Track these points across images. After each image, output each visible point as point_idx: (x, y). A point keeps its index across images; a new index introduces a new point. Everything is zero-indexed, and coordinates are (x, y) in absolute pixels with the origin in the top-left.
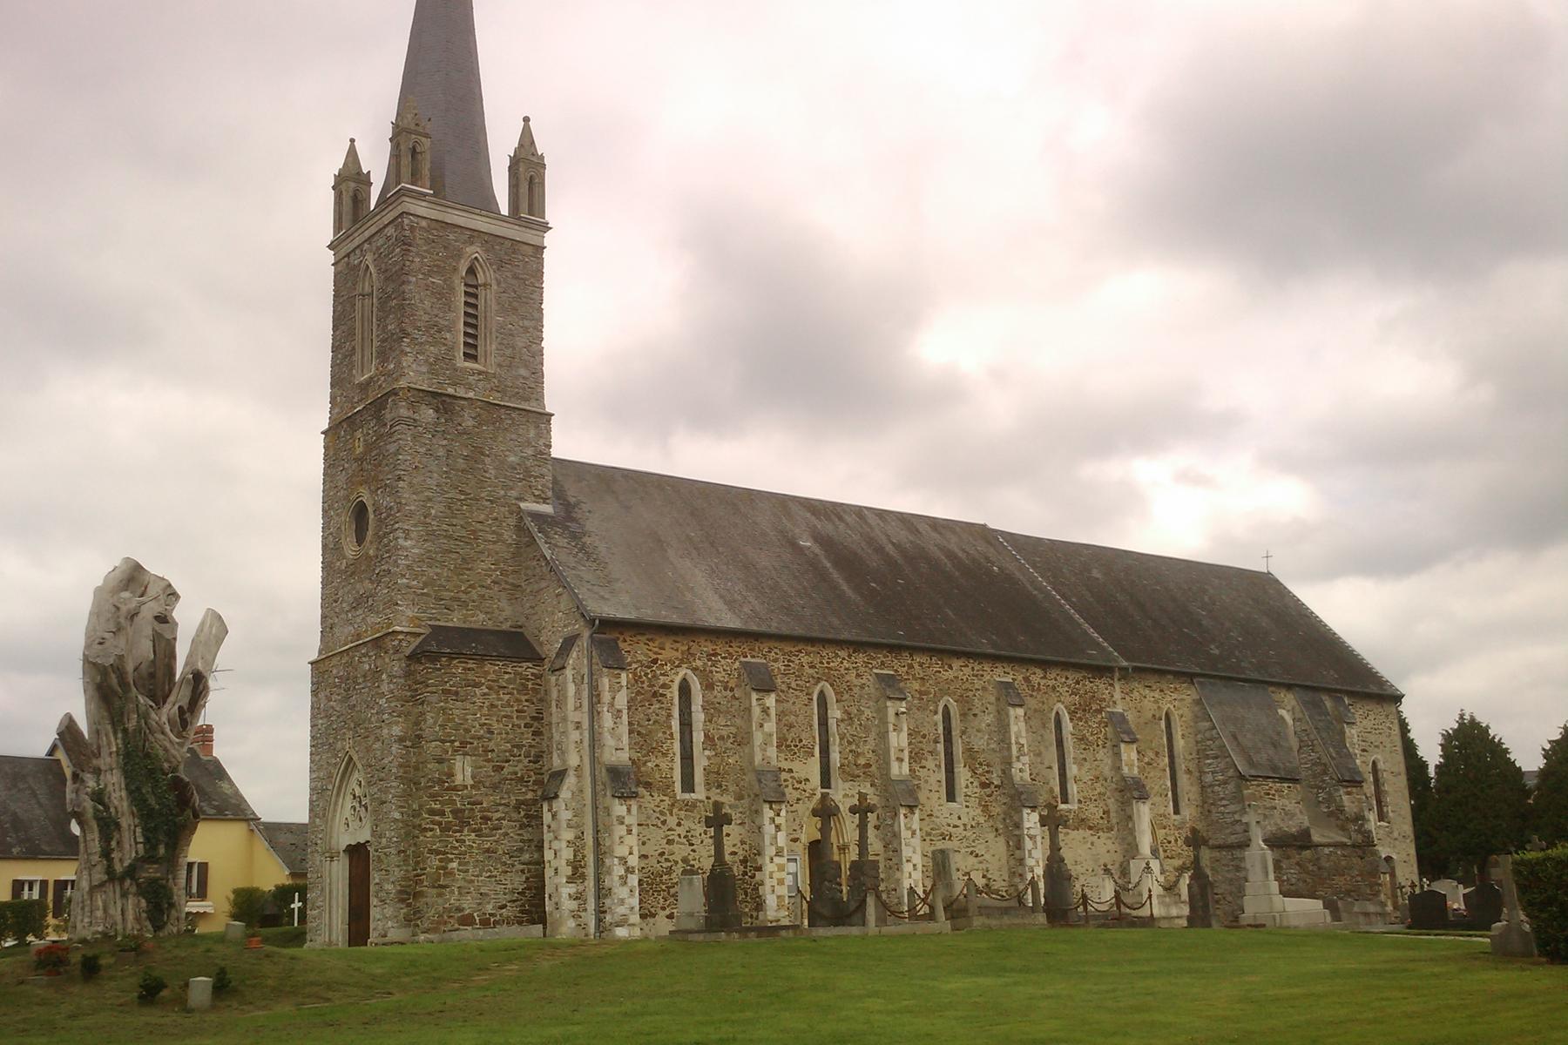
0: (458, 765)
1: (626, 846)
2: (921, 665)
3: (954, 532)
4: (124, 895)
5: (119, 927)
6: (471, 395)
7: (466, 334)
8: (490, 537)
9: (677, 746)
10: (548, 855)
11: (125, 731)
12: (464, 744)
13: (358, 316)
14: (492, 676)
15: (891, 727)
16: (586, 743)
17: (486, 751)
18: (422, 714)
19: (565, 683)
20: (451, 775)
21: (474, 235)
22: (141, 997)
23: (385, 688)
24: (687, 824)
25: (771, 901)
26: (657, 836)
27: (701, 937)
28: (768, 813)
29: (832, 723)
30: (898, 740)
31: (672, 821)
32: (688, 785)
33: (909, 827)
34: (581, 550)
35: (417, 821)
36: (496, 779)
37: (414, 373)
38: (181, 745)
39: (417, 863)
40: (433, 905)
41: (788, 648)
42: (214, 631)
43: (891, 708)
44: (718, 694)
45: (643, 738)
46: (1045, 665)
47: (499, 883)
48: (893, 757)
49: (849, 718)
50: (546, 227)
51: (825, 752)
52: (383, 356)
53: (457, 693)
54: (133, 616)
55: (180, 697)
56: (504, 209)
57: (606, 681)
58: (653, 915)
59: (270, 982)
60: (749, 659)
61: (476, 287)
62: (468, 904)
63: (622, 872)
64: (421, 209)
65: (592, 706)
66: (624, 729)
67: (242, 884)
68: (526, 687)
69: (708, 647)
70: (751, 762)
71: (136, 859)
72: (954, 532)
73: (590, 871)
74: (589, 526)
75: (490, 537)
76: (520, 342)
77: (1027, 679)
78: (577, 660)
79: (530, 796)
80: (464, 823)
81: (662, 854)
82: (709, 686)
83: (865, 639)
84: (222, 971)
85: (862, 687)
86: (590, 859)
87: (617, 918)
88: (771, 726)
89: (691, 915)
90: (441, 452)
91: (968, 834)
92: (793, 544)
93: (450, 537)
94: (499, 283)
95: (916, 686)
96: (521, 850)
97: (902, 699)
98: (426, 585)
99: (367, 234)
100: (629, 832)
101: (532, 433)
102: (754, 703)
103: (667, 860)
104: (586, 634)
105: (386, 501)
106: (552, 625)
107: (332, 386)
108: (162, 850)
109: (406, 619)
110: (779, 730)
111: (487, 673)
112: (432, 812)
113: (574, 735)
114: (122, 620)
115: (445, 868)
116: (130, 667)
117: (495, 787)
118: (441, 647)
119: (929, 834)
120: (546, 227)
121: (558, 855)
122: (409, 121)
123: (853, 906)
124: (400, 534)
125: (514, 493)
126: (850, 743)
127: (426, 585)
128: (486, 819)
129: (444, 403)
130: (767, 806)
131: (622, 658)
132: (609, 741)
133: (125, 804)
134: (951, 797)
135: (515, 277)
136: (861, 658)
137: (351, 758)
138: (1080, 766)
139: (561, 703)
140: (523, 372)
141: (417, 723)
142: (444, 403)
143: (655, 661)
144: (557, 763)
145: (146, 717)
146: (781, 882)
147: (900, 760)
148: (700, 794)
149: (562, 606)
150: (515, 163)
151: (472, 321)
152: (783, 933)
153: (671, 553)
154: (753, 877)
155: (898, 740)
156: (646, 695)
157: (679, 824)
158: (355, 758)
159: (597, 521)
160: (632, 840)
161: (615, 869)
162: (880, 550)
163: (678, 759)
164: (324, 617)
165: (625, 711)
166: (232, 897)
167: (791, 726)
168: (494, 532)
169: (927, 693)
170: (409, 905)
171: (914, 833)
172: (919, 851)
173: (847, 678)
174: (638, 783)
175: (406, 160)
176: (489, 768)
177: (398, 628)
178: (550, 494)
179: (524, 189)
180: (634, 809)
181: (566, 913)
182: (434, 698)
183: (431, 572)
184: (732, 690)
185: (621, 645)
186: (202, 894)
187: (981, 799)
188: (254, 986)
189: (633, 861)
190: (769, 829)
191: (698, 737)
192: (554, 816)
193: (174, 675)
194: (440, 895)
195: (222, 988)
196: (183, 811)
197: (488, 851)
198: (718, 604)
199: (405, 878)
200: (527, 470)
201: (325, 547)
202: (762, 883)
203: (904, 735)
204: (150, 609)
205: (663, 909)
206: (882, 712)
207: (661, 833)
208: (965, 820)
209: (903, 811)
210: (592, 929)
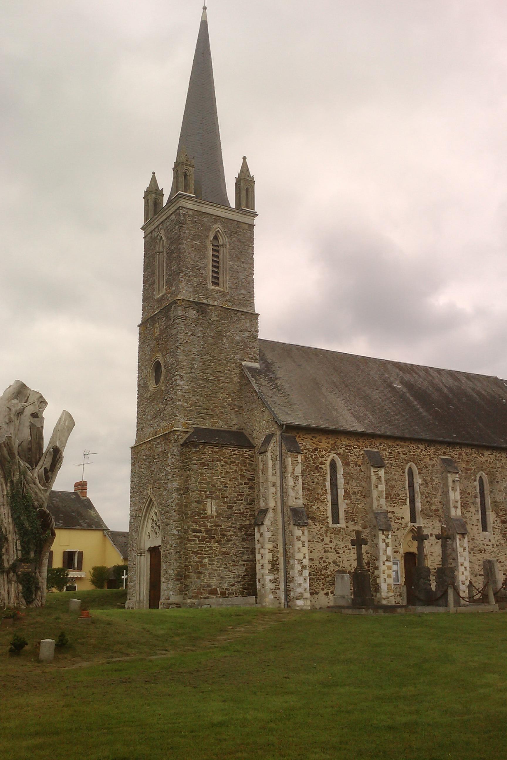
0: (209, 504)
1: (302, 553)
2: (466, 453)
3: (479, 381)
4: (9, 582)
5: (6, 602)
6: (216, 303)
7: (213, 271)
8: (226, 380)
9: (329, 497)
10: (258, 557)
11: (12, 482)
12: (212, 493)
13: (157, 264)
14: (227, 456)
16: (279, 494)
17: (224, 497)
18: (189, 476)
19: (267, 460)
20: (205, 510)
21: (217, 219)
22: (11, 651)
23: (169, 461)
24: (335, 542)
25: (384, 587)
26: (319, 547)
27: (350, 611)
28: (381, 536)
29: (416, 486)
30: (455, 496)
31: (327, 540)
32: (336, 519)
33: (461, 545)
34: (275, 387)
35: (186, 535)
36: (230, 512)
37: (185, 292)
38: (46, 491)
39: (186, 559)
40: (195, 582)
41: (391, 443)
42: (67, 423)
43: (451, 478)
44: (352, 468)
45: (310, 492)
47: (231, 571)
48: (452, 506)
49: (426, 483)
50: (255, 215)
52: (169, 284)
53: (208, 465)
54: (20, 413)
55: (45, 462)
56: (233, 205)
57: (289, 459)
58: (317, 593)
59: (93, 641)
60: (369, 449)
61: (218, 246)
62: (214, 583)
63: (300, 568)
64: (189, 205)
65: (282, 473)
66: (300, 486)
67: (98, 564)
68: (245, 463)
69: (346, 442)
70: (371, 507)
71: (17, 560)
72: (479, 381)
73: (281, 567)
74: (279, 375)
75: (226, 380)
76: (242, 276)
78: (273, 447)
79: (247, 523)
80: (211, 537)
82: (346, 464)
83: (434, 438)
84: (62, 635)
85: (433, 465)
86: (281, 560)
87: (297, 595)
88: (382, 487)
89: (343, 597)
90: (200, 334)
91: (495, 550)
92: (390, 386)
93: (204, 380)
94: (230, 244)
95: (464, 465)
96: (243, 553)
97: (458, 473)
98: (192, 405)
99: (161, 220)
100: (304, 545)
102: (372, 474)
103: (324, 562)
104: (278, 433)
105: (171, 360)
106: (260, 428)
107: (143, 301)
108: (32, 555)
109: (181, 424)
110: (386, 489)
111: (224, 454)
112: (194, 531)
113: (272, 490)
114: (12, 416)
115: (201, 562)
116: (16, 444)
117: (228, 517)
118: (200, 439)
119: (472, 550)
120: (255, 215)
121: (264, 557)
122: (183, 159)
123: (439, 594)
124: (178, 378)
125: (239, 357)
127: (192, 405)
128: (224, 535)
129: (202, 308)
130: (380, 533)
131: (299, 447)
132: (291, 493)
133: (11, 526)
134: (485, 529)
135: (239, 241)
136: (432, 450)
137: (151, 500)
139: (265, 471)
140: (243, 291)
141: (186, 481)
142: (202, 308)
143: (316, 449)
144: (262, 505)
145: (25, 474)
146: (389, 577)
148: (342, 524)
149: (265, 419)
150: (239, 181)
151: (216, 264)
152: (399, 610)
153: (324, 390)
154: (373, 572)
155: (455, 496)
156: (312, 468)
157: (331, 542)
158: (153, 499)
159: (283, 372)
160: (305, 550)
161: (297, 568)
162: (439, 390)
163: (330, 504)
164: (138, 423)
165: (300, 477)
166: (92, 571)
167: (393, 487)
168: (228, 377)
169: (470, 469)
170: (181, 583)
171: (464, 549)
172: (467, 559)
173: (425, 460)
174: (308, 517)
175: (181, 179)
176: (225, 506)
177: (177, 429)
178: (258, 357)
179: (243, 194)
180: (306, 532)
181: (268, 591)
182: (195, 467)
183: (194, 399)
184: (360, 466)
185: (297, 439)
186: (80, 568)
187: (501, 530)
188: (82, 644)
189: (306, 562)
190: (382, 545)
191: (341, 492)
192: (261, 535)
193: (41, 449)
194: (198, 577)
195: (62, 645)
196: (45, 531)
197: (224, 553)
198: (350, 418)
199: (180, 567)
200: (245, 344)
201: (139, 386)
202: (378, 576)
203: (458, 493)
204: (29, 410)
205: (323, 590)
206: (445, 480)
208: (493, 541)
209: (458, 536)
210: (283, 600)
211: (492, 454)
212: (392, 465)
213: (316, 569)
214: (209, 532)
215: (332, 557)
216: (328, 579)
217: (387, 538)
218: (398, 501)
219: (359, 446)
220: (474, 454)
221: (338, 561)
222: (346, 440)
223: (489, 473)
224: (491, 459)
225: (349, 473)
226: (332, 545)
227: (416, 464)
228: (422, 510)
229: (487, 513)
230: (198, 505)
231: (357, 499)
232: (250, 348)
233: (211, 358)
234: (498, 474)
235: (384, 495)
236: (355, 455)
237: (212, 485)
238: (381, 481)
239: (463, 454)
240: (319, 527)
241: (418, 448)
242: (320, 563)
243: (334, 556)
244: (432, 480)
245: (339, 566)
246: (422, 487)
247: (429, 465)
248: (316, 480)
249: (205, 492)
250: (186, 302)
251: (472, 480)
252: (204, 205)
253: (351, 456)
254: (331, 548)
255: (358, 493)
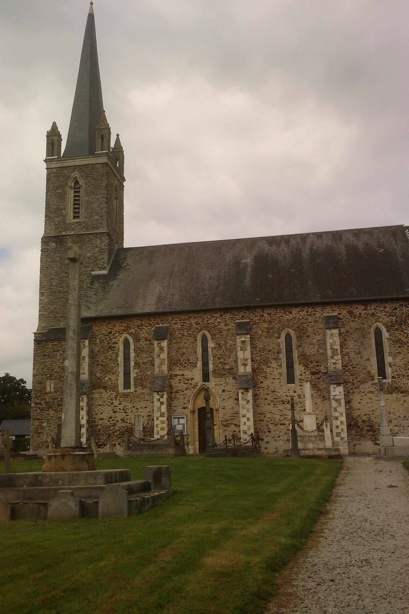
0: (48, 384)
2: (269, 314)
6: (73, 233)
12: (51, 375)
15: (239, 349)
20: (45, 388)
24: (124, 404)
31: (116, 403)
32: (127, 385)
41: (182, 317)
46: (365, 303)
48: (240, 363)
50: (46, 161)
51: (205, 364)
53: (49, 355)
60: (161, 325)
77: (350, 313)
81: (111, 418)
82: (137, 340)
85: (228, 330)
88: (164, 356)
90: (58, 259)
93: (62, 292)
98: (50, 313)
101: (98, 242)
103: (113, 420)
120: (46, 161)
125: (89, 269)
126: (219, 359)
127: (50, 313)
138: (394, 356)
140: (96, 217)
143: (110, 333)
147: (245, 365)
157: (120, 404)
167: (184, 354)
184: (150, 340)
191: (132, 364)
194: (38, 437)
200: (96, 258)
207: (110, 408)
211: (303, 311)
212: (183, 336)
213: (106, 426)
214: (48, 404)
215: (120, 416)
216: (115, 434)
217: (162, 397)
218: (188, 365)
219: (150, 324)
220: (280, 313)
221: (125, 419)
222: (138, 321)
223: (297, 329)
224: (301, 315)
225: (139, 348)
226: (121, 407)
227: (209, 331)
228: (214, 370)
229: (295, 366)
230: (40, 385)
231: (147, 368)
232: (99, 260)
233: (67, 275)
234: (310, 328)
235: (166, 363)
236: (146, 332)
237: (51, 370)
238: (163, 351)
239: (266, 315)
240: (110, 393)
241: (213, 316)
242: (109, 421)
243: (123, 415)
244: (226, 343)
245: (127, 422)
246: (215, 350)
247: (224, 330)
248: (110, 357)
249: (46, 375)
250: (48, 238)
251: (275, 337)
252: (65, 161)
253: (142, 333)
254: (120, 409)
255: (148, 362)
